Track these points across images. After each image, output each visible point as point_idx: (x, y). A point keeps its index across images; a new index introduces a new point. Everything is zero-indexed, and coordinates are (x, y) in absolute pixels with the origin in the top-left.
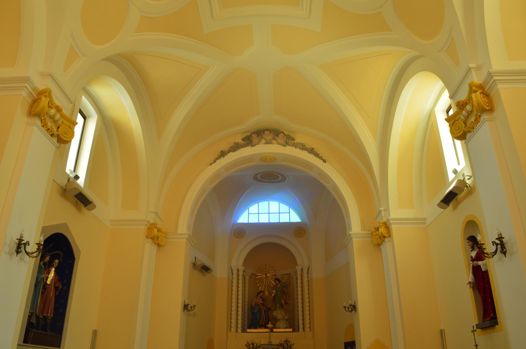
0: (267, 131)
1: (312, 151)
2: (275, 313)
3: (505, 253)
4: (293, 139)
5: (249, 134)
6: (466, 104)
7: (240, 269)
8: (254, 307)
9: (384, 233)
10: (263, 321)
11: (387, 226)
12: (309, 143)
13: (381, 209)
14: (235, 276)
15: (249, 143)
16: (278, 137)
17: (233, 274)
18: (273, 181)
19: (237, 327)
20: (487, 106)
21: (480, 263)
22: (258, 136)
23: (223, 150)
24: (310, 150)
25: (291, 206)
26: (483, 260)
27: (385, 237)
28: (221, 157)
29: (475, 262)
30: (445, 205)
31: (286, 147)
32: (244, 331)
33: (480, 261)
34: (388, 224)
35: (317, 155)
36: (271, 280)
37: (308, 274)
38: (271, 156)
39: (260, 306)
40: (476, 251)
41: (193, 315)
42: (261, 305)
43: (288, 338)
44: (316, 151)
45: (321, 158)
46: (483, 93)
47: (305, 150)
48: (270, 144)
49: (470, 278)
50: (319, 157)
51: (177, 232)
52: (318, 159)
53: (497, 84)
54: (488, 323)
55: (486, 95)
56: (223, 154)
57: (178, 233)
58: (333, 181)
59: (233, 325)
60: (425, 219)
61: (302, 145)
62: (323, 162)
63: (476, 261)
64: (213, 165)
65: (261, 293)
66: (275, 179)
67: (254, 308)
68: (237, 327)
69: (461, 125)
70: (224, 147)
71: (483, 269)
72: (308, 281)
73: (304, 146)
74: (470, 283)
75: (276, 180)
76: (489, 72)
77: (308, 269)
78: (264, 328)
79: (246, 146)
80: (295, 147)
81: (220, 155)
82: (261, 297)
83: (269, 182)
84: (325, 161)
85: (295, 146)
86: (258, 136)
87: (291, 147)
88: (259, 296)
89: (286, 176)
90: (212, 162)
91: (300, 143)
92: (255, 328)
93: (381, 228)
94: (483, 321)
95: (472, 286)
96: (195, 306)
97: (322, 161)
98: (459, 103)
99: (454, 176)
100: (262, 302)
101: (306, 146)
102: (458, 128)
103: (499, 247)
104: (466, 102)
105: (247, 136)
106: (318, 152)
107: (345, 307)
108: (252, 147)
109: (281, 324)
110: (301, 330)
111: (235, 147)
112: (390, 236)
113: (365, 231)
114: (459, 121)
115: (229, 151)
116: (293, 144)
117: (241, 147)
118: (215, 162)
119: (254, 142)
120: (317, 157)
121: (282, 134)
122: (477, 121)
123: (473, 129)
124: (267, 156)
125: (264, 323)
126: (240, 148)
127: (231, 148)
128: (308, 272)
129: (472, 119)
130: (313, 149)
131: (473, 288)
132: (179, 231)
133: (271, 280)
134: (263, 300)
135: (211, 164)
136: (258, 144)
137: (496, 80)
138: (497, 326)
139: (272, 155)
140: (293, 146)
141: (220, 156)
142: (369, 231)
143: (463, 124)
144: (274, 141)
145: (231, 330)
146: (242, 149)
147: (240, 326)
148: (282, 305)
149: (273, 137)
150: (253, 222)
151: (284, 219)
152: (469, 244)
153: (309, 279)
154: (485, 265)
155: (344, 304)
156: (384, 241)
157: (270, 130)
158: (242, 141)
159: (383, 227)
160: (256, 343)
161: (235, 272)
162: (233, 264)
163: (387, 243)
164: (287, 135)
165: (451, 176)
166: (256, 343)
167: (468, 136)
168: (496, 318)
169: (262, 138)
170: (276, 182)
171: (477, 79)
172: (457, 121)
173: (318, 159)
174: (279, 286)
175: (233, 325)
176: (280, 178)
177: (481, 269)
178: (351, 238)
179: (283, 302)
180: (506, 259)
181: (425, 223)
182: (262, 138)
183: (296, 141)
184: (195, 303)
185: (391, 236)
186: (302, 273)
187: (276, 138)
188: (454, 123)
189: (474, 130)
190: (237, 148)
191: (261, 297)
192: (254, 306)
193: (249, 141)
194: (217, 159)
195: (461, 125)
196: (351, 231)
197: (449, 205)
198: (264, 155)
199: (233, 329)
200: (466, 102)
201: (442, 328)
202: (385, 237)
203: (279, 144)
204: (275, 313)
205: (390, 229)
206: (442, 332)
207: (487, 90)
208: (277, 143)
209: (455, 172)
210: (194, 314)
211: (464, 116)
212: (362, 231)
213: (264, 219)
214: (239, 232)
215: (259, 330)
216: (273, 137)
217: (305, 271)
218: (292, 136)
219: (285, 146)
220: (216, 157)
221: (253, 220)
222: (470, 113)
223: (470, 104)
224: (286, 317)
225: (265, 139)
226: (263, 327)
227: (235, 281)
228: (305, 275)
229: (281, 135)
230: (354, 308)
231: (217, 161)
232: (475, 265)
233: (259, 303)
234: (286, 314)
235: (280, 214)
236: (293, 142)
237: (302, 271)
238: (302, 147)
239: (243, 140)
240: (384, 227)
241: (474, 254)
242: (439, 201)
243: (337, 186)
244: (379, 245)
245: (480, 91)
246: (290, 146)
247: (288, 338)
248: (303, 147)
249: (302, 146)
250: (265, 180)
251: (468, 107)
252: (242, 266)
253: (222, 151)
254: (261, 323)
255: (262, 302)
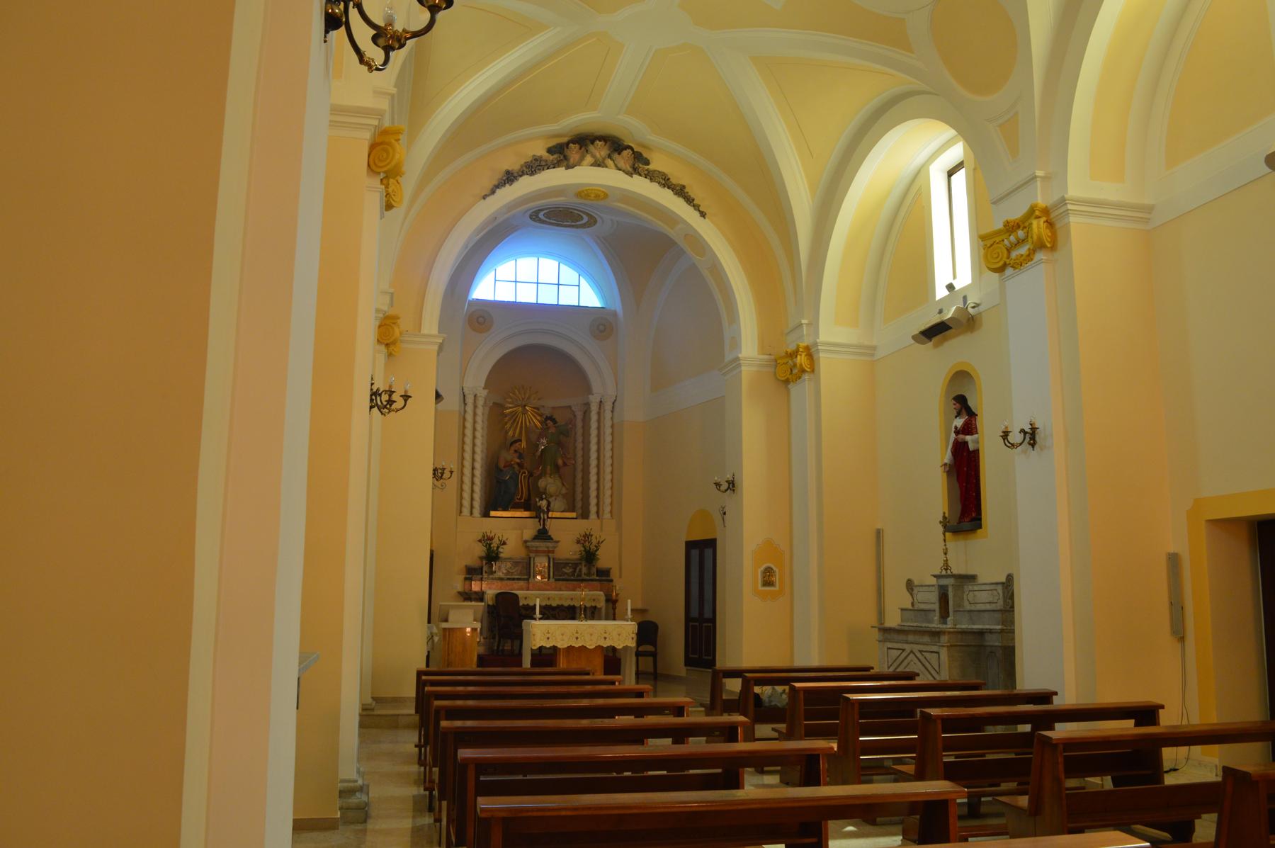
0: (600, 141)
1: (680, 191)
2: (542, 483)
3: (1033, 445)
4: (647, 162)
5: (565, 140)
6: (1019, 227)
7: (479, 395)
8: (503, 469)
9: (804, 366)
10: (522, 497)
11: (810, 352)
12: (679, 175)
13: (803, 321)
14: (470, 409)
15: (562, 160)
16: (619, 154)
17: (465, 404)
18: (565, 223)
19: (472, 507)
20: (1049, 242)
21: (968, 438)
22: (580, 149)
23: (510, 169)
24: (678, 188)
25: (582, 271)
26: (972, 434)
27: (803, 371)
28: (505, 184)
29: (961, 437)
30: (926, 339)
31: (632, 177)
32: (486, 514)
33: (968, 435)
34: (813, 350)
35: (689, 200)
36: (533, 418)
37: (612, 412)
38: (600, 191)
39: (514, 468)
40: (964, 419)
41: (440, 486)
42: (516, 466)
43: (591, 529)
44: (687, 193)
45: (696, 207)
46: (1047, 221)
47: (668, 188)
48: (603, 167)
49: (948, 457)
50: (694, 206)
51: (420, 332)
52: (690, 209)
53: (1070, 212)
54: (966, 525)
55: (1050, 224)
56: (509, 178)
57: (422, 332)
58: (711, 250)
59: (466, 503)
60: (874, 348)
61: (664, 177)
62: (701, 216)
63: (963, 434)
64: (490, 199)
65: (517, 444)
66: (572, 222)
67: (501, 471)
68: (472, 507)
69: (1002, 252)
70: (513, 164)
71: (971, 447)
72: (612, 426)
73: (669, 179)
74: (945, 464)
75: (573, 224)
76: (1063, 197)
77: (613, 403)
78: (522, 510)
79: (555, 165)
80: (651, 179)
81: (505, 181)
82: (516, 451)
83: (558, 225)
84: (703, 215)
85: (651, 176)
86: (580, 149)
87: (643, 178)
88: (513, 448)
89: (597, 217)
90: (487, 193)
91: (659, 172)
92: (505, 509)
93: (801, 355)
94: (959, 522)
95: (947, 469)
96: (445, 469)
97: (697, 214)
98: (1008, 222)
99: (946, 293)
100: (518, 461)
101: (671, 180)
102: (996, 256)
103: (1028, 437)
104: (1018, 224)
105: (558, 144)
106: (692, 196)
107: (718, 485)
108: (566, 169)
109: (557, 504)
110: (593, 515)
111: (534, 166)
112: (813, 371)
113: (764, 354)
114: (1001, 246)
115: (522, 174)
116: (646, 172)
117: (546, 168)
118: (493, 192)
119: (572, 160)
120: (689, 204)
121: (629, 151)
122: (1029, 257)
123: (1021, 265)
124: (592, 190)
125: (523, 501)
126: (543, 170)
127: (526, 167)
128: (613, 407)
129: (1023, 250)
130: (684, 187)
131: (949, 473)
132: (425, 330)
133: (533, 418)
134: (520, 456)
135: (484, 197)
136: (579, 165)
137: (1071, 210)
138: (979, 531)
139: (604, 190)
140: (646, 178)
141: (503, 182)
142: (770, 355)
143: (1005, 252)
144: (609, 162)
145: (461, 512)
146: (548, 170)
147: (477, 504)
148: (557, 468)
149: (608, 152)
150: (506, 300)
151: (568, 298)
152: (954, 406)
153: (615, 421)
154: (977, 442)
155: (716, 478)
156: (800, 378)
157: (604, 138)
158: (547, 154)
159: (804, 354)
160: (499, 537)
161: (470, 400)
162: (468, 384)
163: (807, 382)
164: (637, 152)
165: (941, 292)
166: (499, 537)
167: (1009, 271)
168: (980, 519)
169: (587, 151)
170: (577, 227)
171: (1042, 199)
172: (998, 245)
173: (692, 209)
174: (552, 430)
175: (466, 503)
176: (586, 219)
177: (968, 446)
178: (740, 365)
179: (560, 462)
180: (1033, 454)
181: (873, 355)
182: (587, 151)
183: (651, 167)
184: (444, 464)
185: (815, 372)
186: (600, 408)
187: (615, 156)
188: (992, 245)
189: (1022, 268)
190: (539, 169)
191: (516, 451)
192: (504, 467)
193: (562, 157)
194: (498, 186)
195: (1002, 252)
196: (741, 352)
197: (931, 341)
198: (588, 188)
199: (466, 511)
200: (1018, 224)
201: (879, 527)
202: (803, 371)
203: (620, 170)
204: (542, 483)
205: (815, 358)
206: (879, 534)
207: (1054, 217)
208: (616, 166)
209: (950, 287)
210: (442, 486)
211: (1010, 242)
212: (758, 354)
213: (527, 295)
214: (481, 320)
215: (514, 512)
216: (608, 152)
217: (608, 407)
218: (645, 155)
219: (631, 175)
220: (496, 183)
221: (505, 294)
222: (1020, 242)
223: (1025, 230)
224: (564, 491)
225: (593, 156)
226: (522, 508)
227: (469, 417)
228: (608, 415)
229: (626, 153)
230: (732, 485)
231: (498, 191)
232: (960, 440)
233: (513, 463)
234: (563, 484)
235: (557, 286)
236: (646, 167)
237: (600, 405)
238: (663, 182)
239: (550, 151)
240: (806, 355)
241: (959, 422)
242: (917, 332)
243: (720, 263)
244: (787, 382)
245: (1044, 219)
246: (640, 175)
247: (591, 529)
248: (665, 181)
249: (664, 180)
250: (551, 221)
251: (1021, 233)
252: (484, 389)
253: (508, 172)
254: (518, 501)
255: (518, 461)
